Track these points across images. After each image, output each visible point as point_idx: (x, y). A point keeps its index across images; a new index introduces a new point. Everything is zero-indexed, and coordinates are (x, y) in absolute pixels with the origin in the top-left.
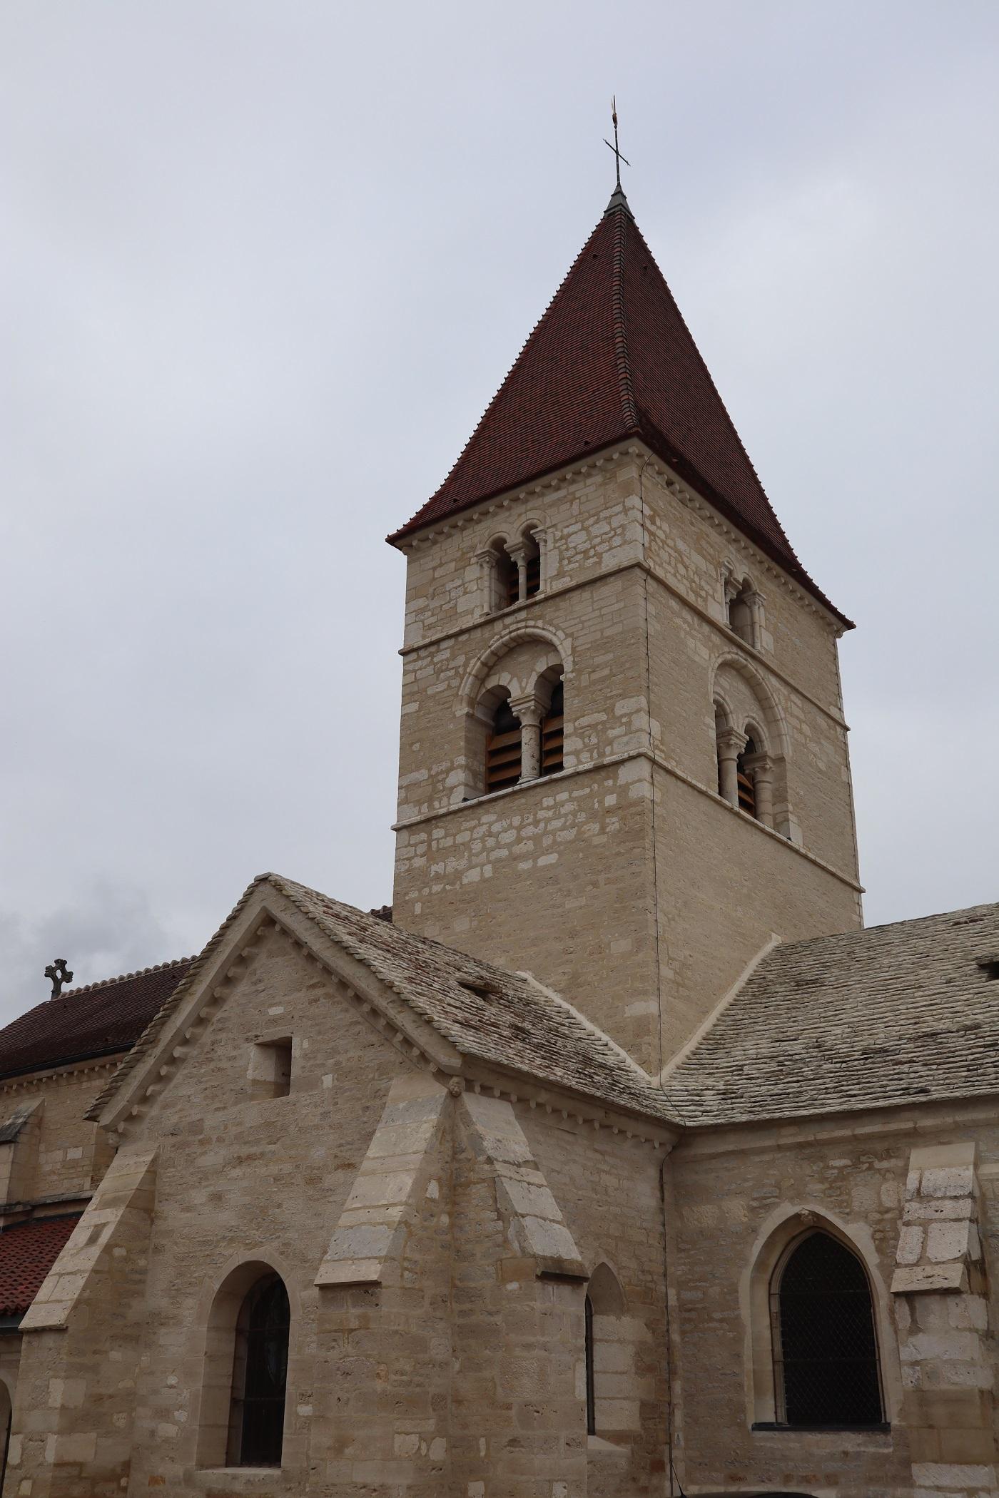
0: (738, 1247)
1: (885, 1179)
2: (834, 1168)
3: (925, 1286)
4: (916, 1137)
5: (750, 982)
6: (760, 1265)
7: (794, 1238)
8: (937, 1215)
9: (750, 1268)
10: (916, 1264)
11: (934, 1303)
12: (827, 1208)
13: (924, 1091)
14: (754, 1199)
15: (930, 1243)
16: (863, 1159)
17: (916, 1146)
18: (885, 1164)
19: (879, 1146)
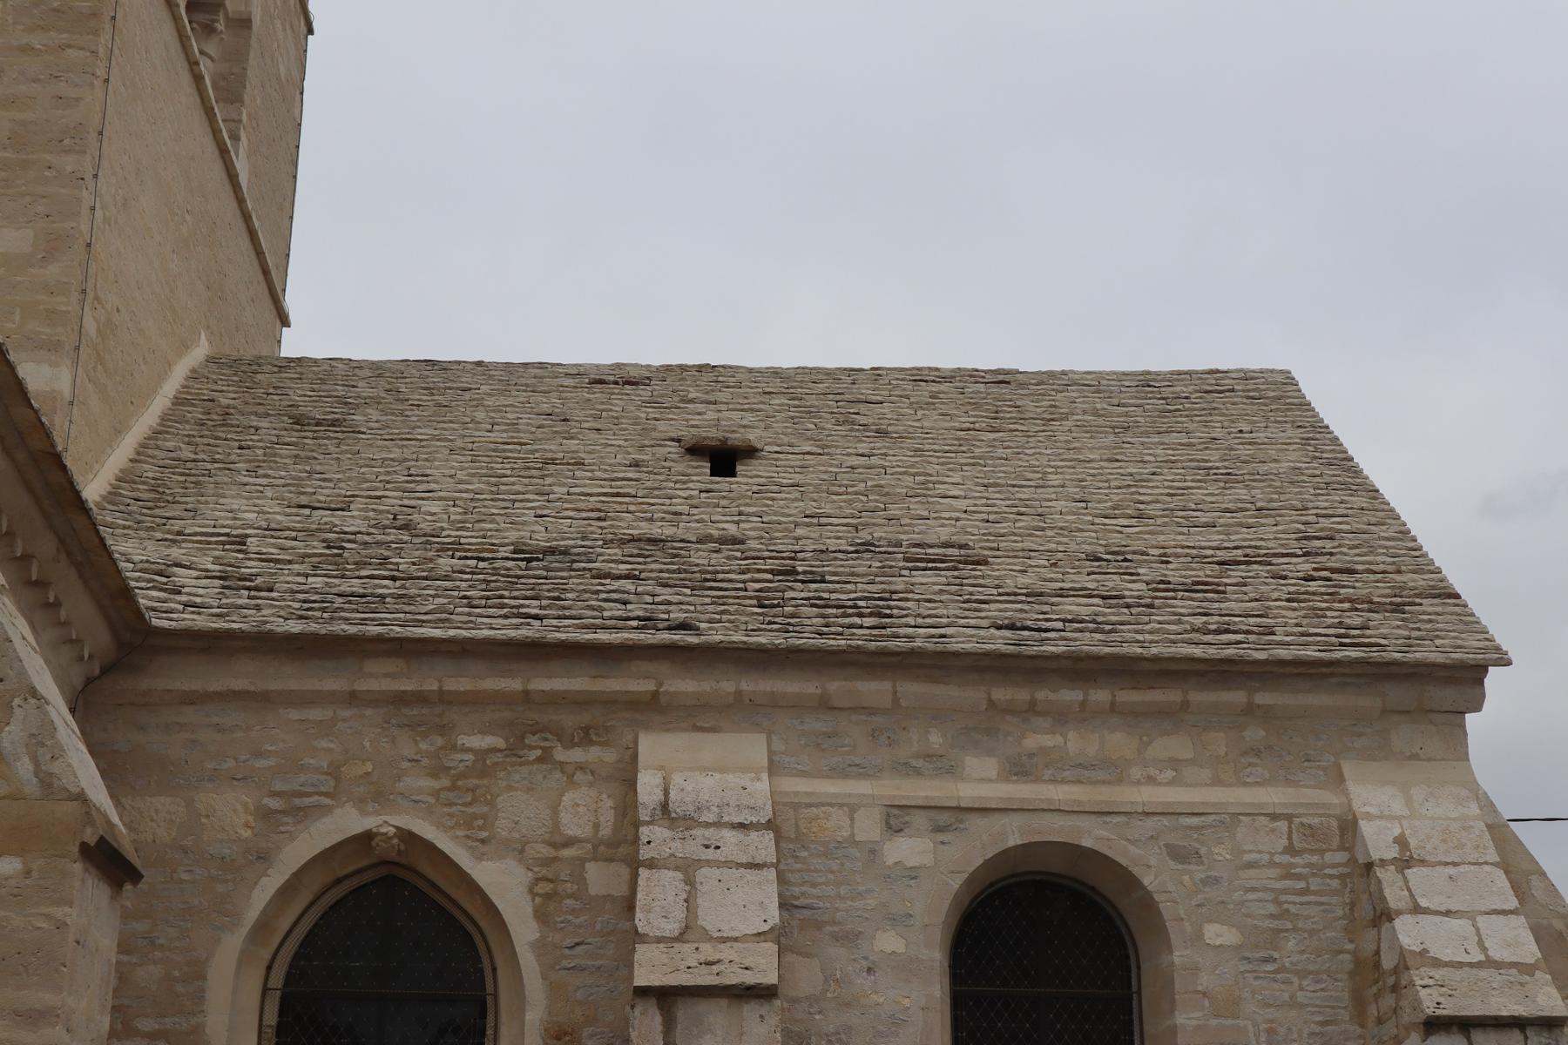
0: (220, 888)
1: (572, 783)
2: (468, 750)
3: (705, 978)
4: (654, 710)
5: (178, 401)
6: (263, 926)
7: (338, 881)
8: (710, 854)
9: (244, 930)
10: (680, 938)
11: (716, 1015)
12: (439, 825)
13: (683, 626)
14: (273, 794)
15: (703, 903)
16: (531, 740)
17: (647, 727)
18: (577, 755)
19: (569, 720)
